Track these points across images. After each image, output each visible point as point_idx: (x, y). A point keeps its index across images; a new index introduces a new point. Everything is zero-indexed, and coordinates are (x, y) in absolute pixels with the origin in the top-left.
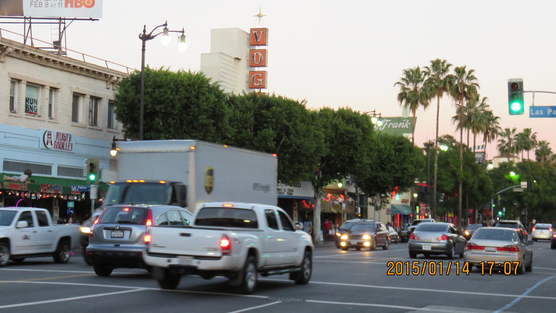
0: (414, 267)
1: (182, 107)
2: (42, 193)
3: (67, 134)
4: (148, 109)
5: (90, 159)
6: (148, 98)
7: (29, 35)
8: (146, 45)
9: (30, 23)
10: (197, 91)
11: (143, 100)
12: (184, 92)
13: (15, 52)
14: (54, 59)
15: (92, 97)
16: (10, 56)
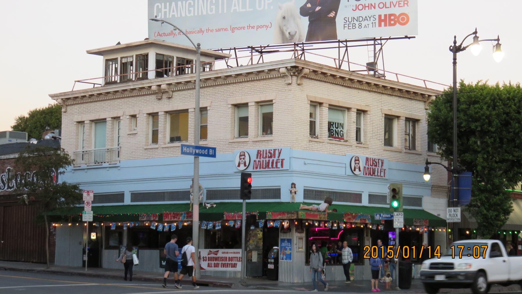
1: (501, 124)
2: (345, 223)
3: (379, 160)
4: (462, 127)
5: (392, 184)
6: (462, 115)
7: (346, 59)
8: (457, 58)
9: (347, 47)
10: (518, 105)
11: (456, 118)
12: (503, 106)
13: (313, 74)
14: (373, 82)
15: (408, 120)
16: (307, 78)
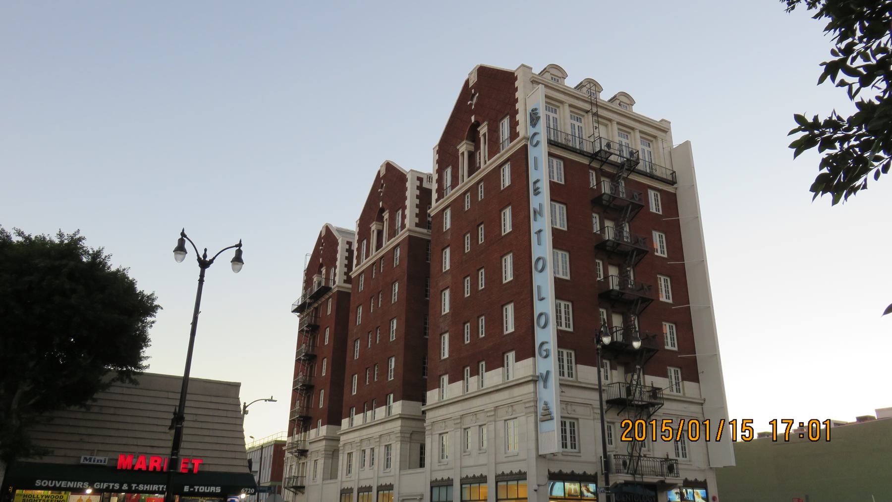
0: (664, 428)
